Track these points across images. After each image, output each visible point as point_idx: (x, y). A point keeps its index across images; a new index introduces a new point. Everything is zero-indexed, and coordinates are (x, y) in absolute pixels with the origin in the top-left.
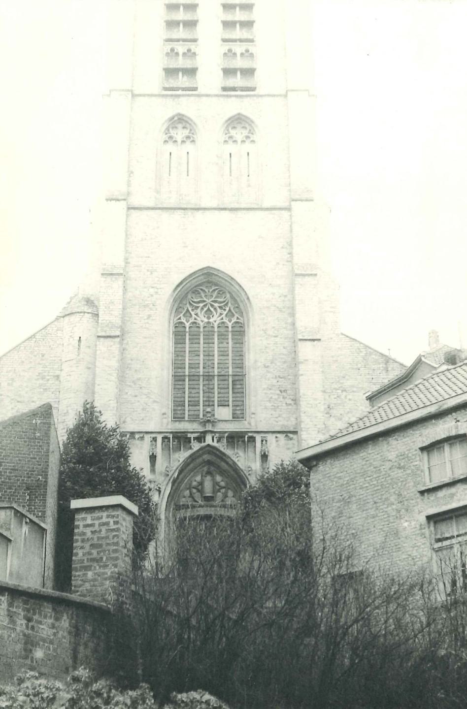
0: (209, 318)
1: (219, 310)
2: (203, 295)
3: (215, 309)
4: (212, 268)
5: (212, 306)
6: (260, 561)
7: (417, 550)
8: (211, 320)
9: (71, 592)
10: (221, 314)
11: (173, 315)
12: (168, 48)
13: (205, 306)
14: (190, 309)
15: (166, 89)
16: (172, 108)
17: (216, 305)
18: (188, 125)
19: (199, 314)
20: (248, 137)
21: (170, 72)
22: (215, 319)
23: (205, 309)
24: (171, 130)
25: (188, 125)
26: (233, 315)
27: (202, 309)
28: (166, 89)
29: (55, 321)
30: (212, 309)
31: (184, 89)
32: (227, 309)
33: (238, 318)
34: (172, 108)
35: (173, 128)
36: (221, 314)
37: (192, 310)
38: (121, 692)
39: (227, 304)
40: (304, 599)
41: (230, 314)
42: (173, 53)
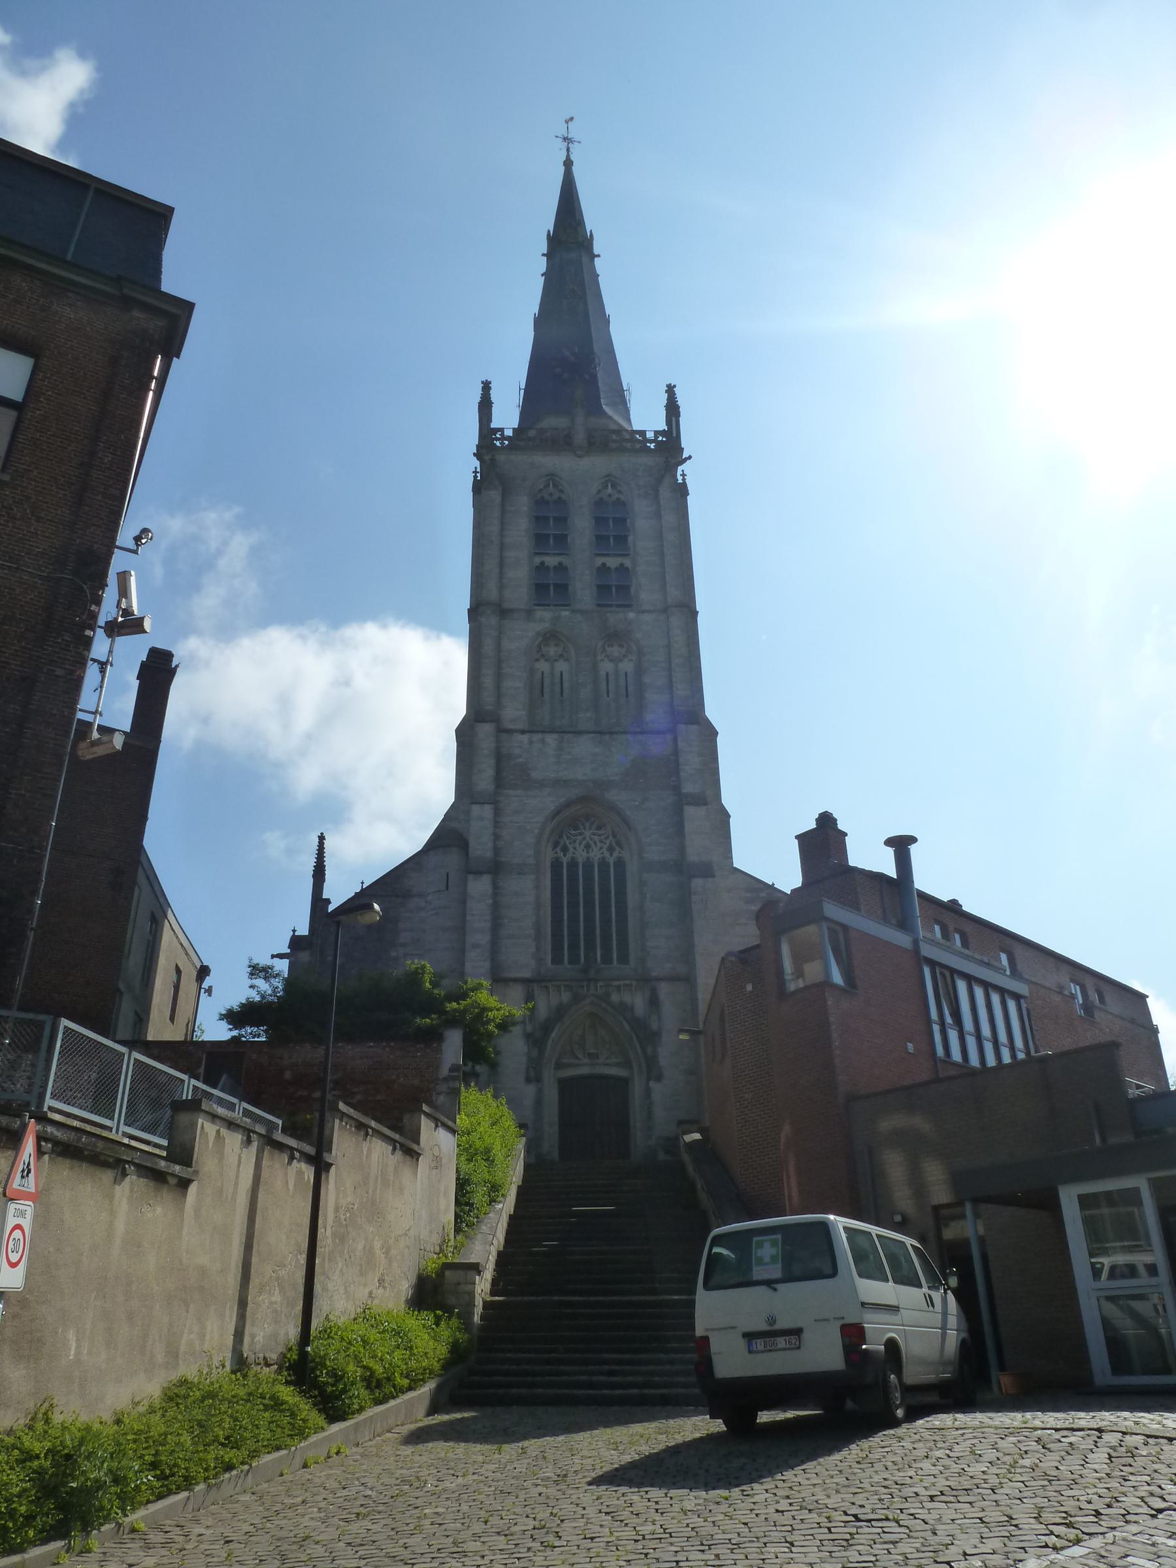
0: (588, 852)
1: (599, 844)
2: (581, 827)
3: (595, 843)
5: (591, 839)
6: (361, 1266)
7: (467, 1225)
9: (336, 1040)
10: (601, 848)
13: (584, 839)
14: (567, 842)
19: (577, 847)
23: (584, 843)
24: (606, 647)
29: (568, 156)
30: (592, 843)
32: (608, 842)
33: (620, 853)
35: (608, 646)
36: (601, 848)
37: (570, 844)
38: (481, 1090)
40: (89, 1483)
41: (611, 849)
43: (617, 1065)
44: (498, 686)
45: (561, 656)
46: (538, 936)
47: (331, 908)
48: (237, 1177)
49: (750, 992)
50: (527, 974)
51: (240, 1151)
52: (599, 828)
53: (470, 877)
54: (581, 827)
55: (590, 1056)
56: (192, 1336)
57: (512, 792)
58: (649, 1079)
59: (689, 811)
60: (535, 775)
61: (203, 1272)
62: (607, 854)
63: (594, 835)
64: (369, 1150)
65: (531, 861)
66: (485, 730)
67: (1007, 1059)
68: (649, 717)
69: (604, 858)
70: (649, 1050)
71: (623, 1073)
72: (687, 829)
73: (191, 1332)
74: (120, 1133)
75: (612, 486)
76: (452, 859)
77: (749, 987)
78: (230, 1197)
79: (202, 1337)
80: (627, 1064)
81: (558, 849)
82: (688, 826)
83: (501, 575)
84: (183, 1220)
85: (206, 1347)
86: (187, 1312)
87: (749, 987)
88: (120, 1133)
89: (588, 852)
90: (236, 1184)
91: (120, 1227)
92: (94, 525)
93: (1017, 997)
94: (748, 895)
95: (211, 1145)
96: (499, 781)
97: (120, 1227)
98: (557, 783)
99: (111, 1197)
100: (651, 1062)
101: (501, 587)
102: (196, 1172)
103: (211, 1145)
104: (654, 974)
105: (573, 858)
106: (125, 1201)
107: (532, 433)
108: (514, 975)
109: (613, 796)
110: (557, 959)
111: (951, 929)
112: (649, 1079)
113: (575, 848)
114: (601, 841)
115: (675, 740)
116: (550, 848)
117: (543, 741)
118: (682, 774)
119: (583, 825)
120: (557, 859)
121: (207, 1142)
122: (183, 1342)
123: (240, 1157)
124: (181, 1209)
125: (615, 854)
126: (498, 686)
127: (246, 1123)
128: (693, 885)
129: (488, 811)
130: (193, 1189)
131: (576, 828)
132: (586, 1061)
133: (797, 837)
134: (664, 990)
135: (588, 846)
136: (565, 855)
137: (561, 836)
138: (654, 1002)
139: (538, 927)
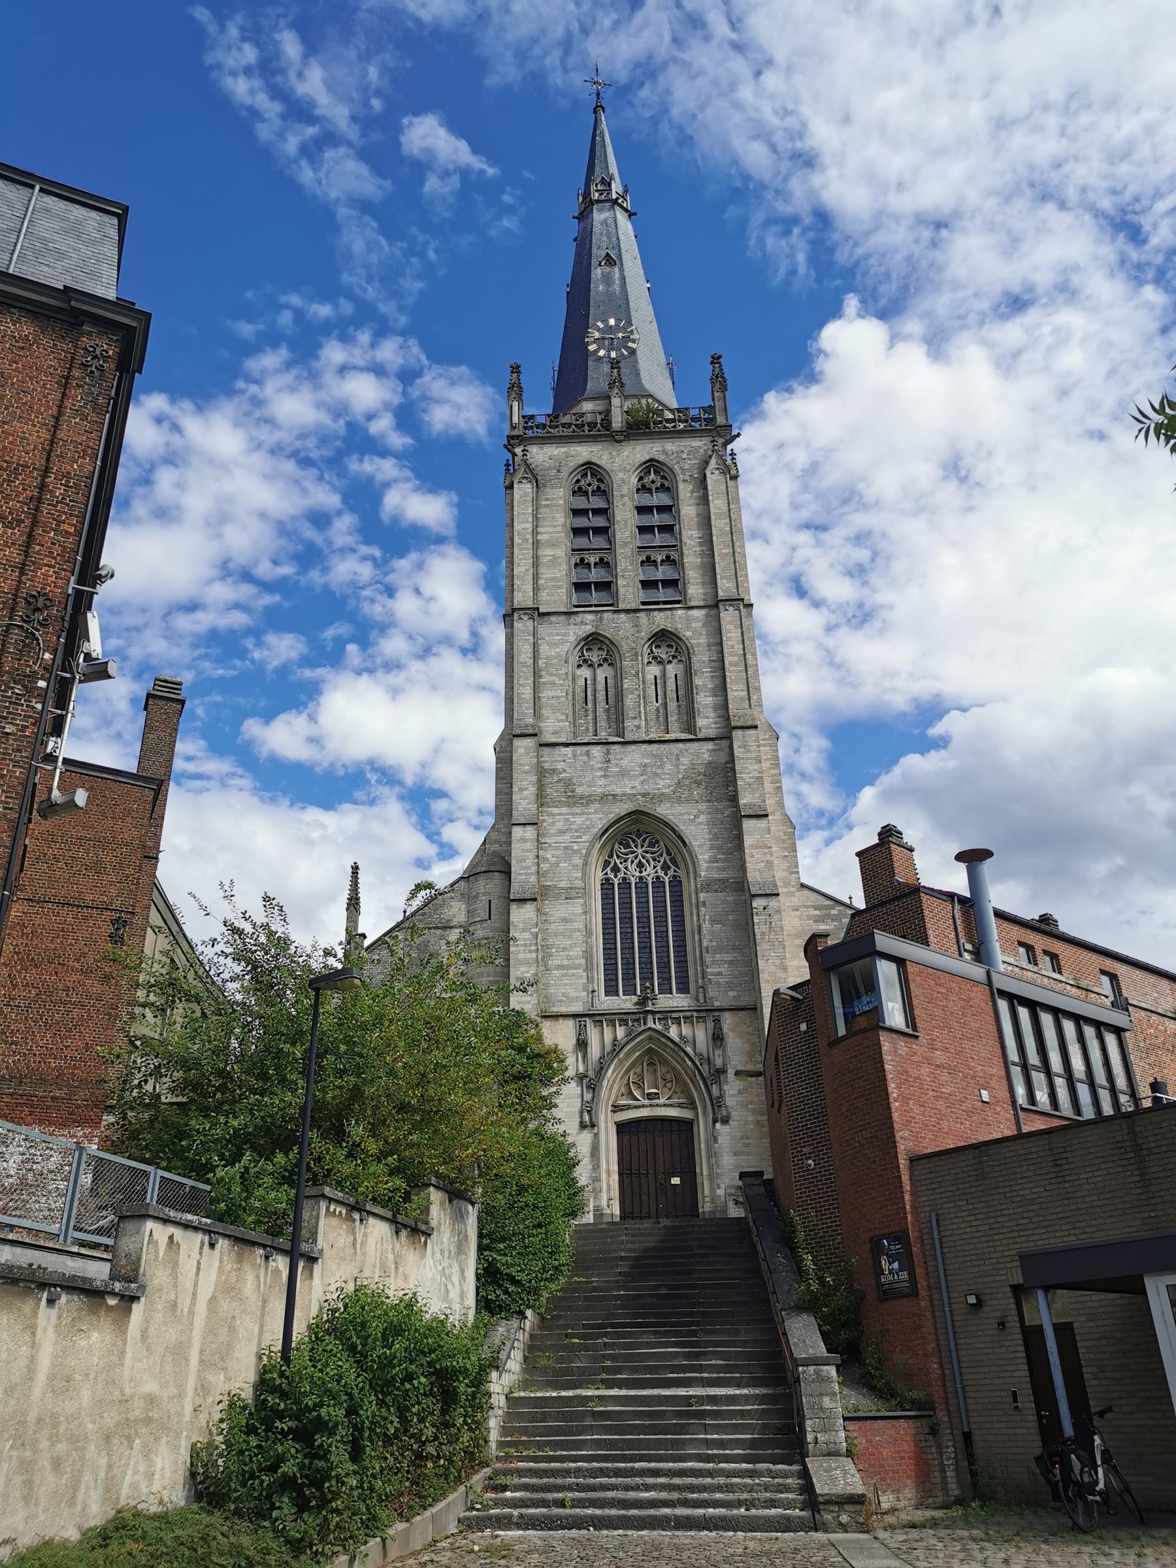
0: (641, 872)
1: (652, 863)
2: (632, 845)
3: (648, 861)
4: (595, 464)
8: (644, 874)
11: (598, 846)
12: (576, 559)
14: (618, 862)
15: (643, 603)
16: (586, 624)
17: (648, 855)
18: (604, 647)
20: (674, 657)
21: (580, 587)
22: (649, 872)
23: (636, 861)
25: (604, 647)
26: (669, 868)
27: (632, 862)
28: (643, 603)
31: (665, 603)
32: (662, 860)
34: (586, 624)
39: (661, 855)
41: (665, 868)
42: (582, 564)
43: (680, 1105)
44: (536, 698)
45: (605, 660)
46: (589, 967)
47: (367, 943)
48: (196, 1285)
49: (805, 1032)
50: (578, 1008)
51: (198, 1257)
52: (651, 845)
53: (514, 906)
54: (632, 845)
55: (650, 1096)
56: (137, 1477)
57: (555, 810)
58: (715, 1121)
59: (748, 824)
60: (579, 791)
61: (151, 1400)
62: (661, 873)
63: (647, 852)
64: (365, 1235)
65: (579, 883)
66: (523, 746)
67: (1108, 1109)
68: (701, 722)
69: (658, 878)
70: (715, 1090)
71: (686, 1114)
72: (746, 844)
73: (135, 1473)
74: (69, 1240)
75: (655, 472)
76: (488, 887)
77: (803, 1027)
78: (186, 1310)
79: (150, 1476)
80: (691, 1105)
81: (608, 870)
82: (748, 841)
83: (536, 577)
84: (125, 1344)
85: (154, 1489)
86: (132, 1448)
87: (803, 1027)
88: (69, 1240)
89: (641, 872)
90: (194, 1295)
91: (45, 1361)
92: (46, 565)
93: (1118, 1031)
94: (818, 912)
95: (161, 1253)
96: (541, 798)
97: (45, 1361)
98: (604, 798)
99: (32, 1329)
100: (717, 1103)
101: (536, 589)
102: (142, 1288)
103: (161, 1253)
104: (717, 1004)
105: (624, 879)
106: (51, 1330)
107: (566, 419)
108: (564, 1009)
109: (664, 810)
110: (611, 990)
111: (1039, 952)
112: (715, 1121)
113: (626, 868)
114: (654, 860)
115: (731, 747)
116: (600, 869)
117: (588, 754)
118: (740, 783)
119: (634, 841)
120: (607, 880)
121: (157, 1251)
122: (126, 1485)
123: (199, 1263)
124: (124, 1332)
125: (671, 873)
126: (536, 698)
127: (206, 1224)
128: (755, 905)
129: (530, 832)
130: (137, 1309)
131: (627, 846)
132: (646, 1102)
133: (859, 854)
134: (728, 1020)
135: (640, 866)
136: (616, 876)
137: (611, 856)
138: (718, 1038)
139: (588, 956)
